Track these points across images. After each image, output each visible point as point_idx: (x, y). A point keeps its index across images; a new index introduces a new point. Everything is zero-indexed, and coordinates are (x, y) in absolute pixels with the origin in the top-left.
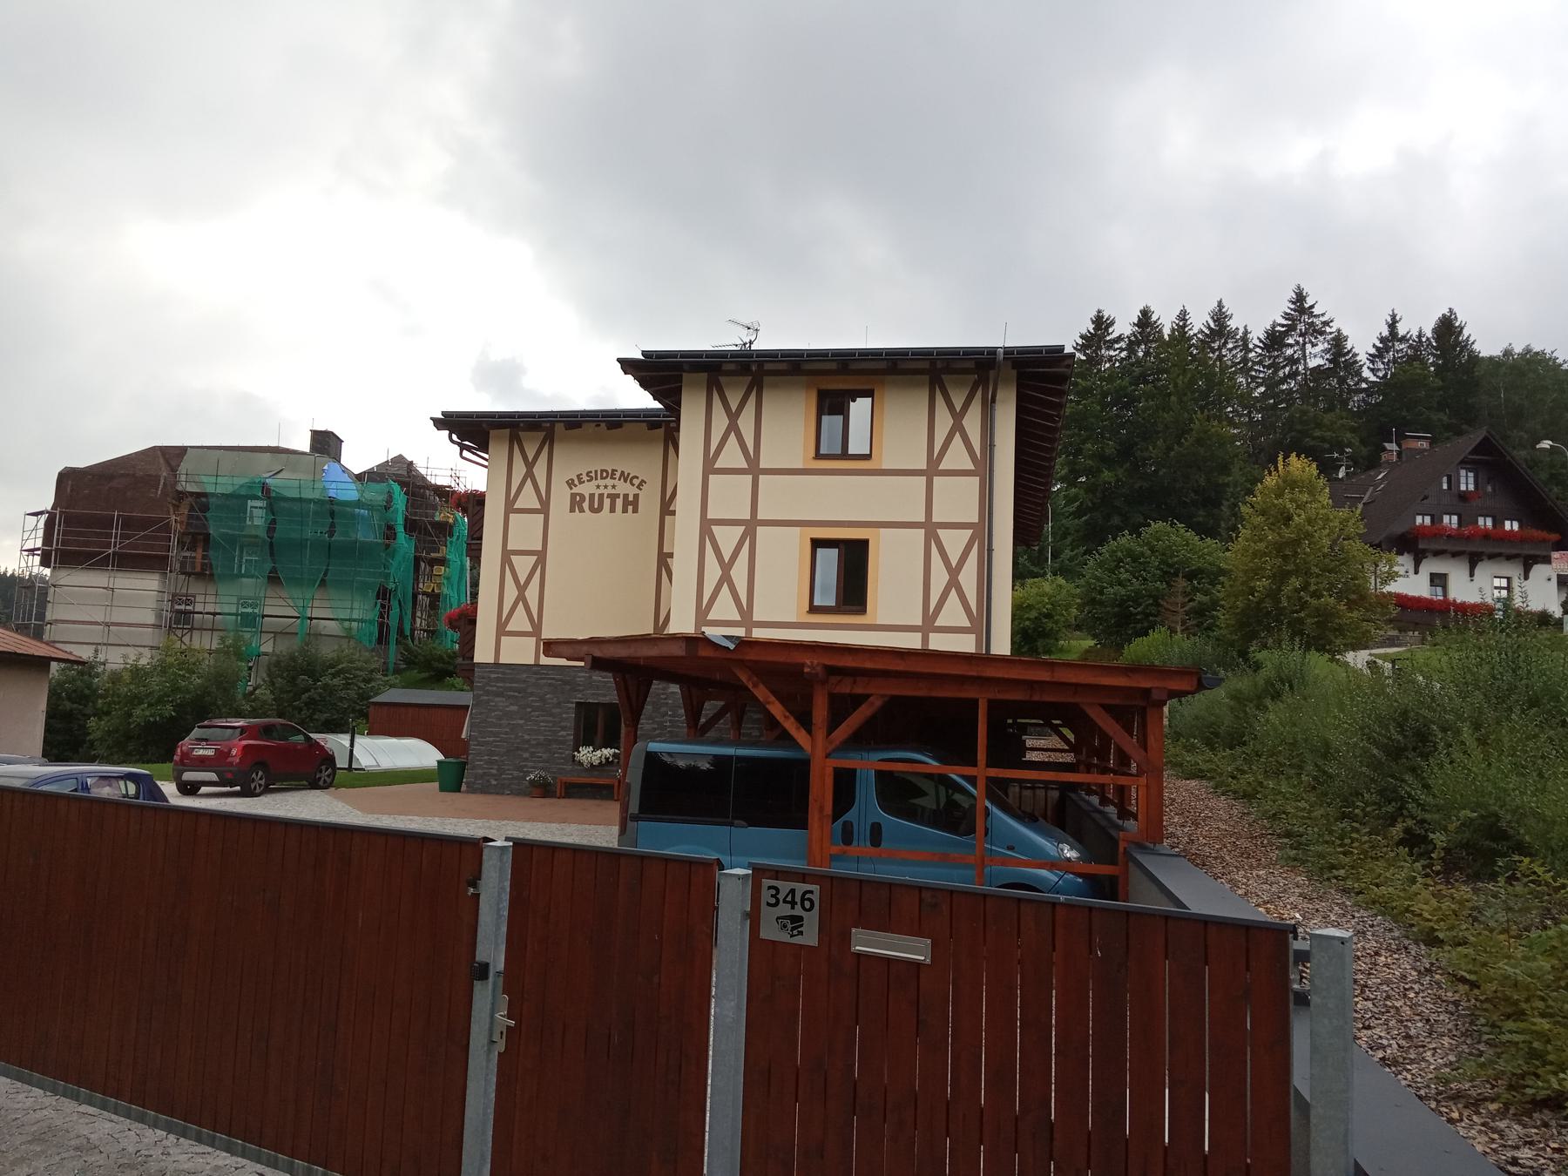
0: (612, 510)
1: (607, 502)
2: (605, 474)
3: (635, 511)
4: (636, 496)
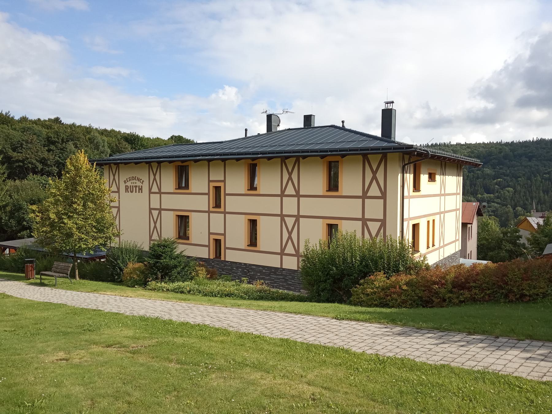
0: (136, 192)
1: (134, 188)
2: (134, 178)
3: (142, 192)
4: (142, 186)
